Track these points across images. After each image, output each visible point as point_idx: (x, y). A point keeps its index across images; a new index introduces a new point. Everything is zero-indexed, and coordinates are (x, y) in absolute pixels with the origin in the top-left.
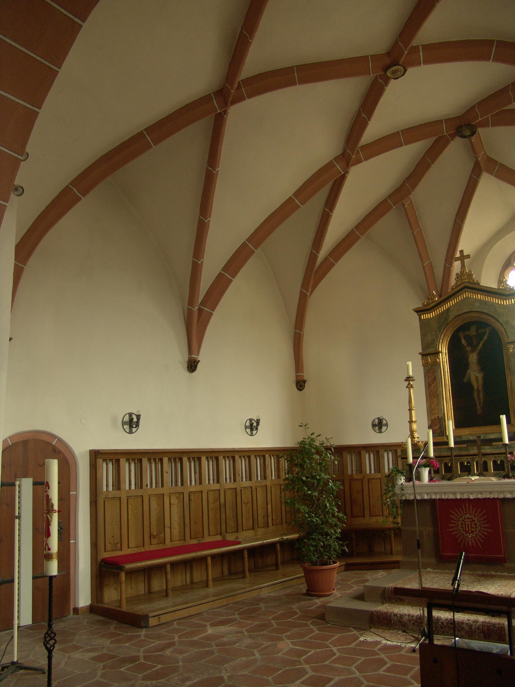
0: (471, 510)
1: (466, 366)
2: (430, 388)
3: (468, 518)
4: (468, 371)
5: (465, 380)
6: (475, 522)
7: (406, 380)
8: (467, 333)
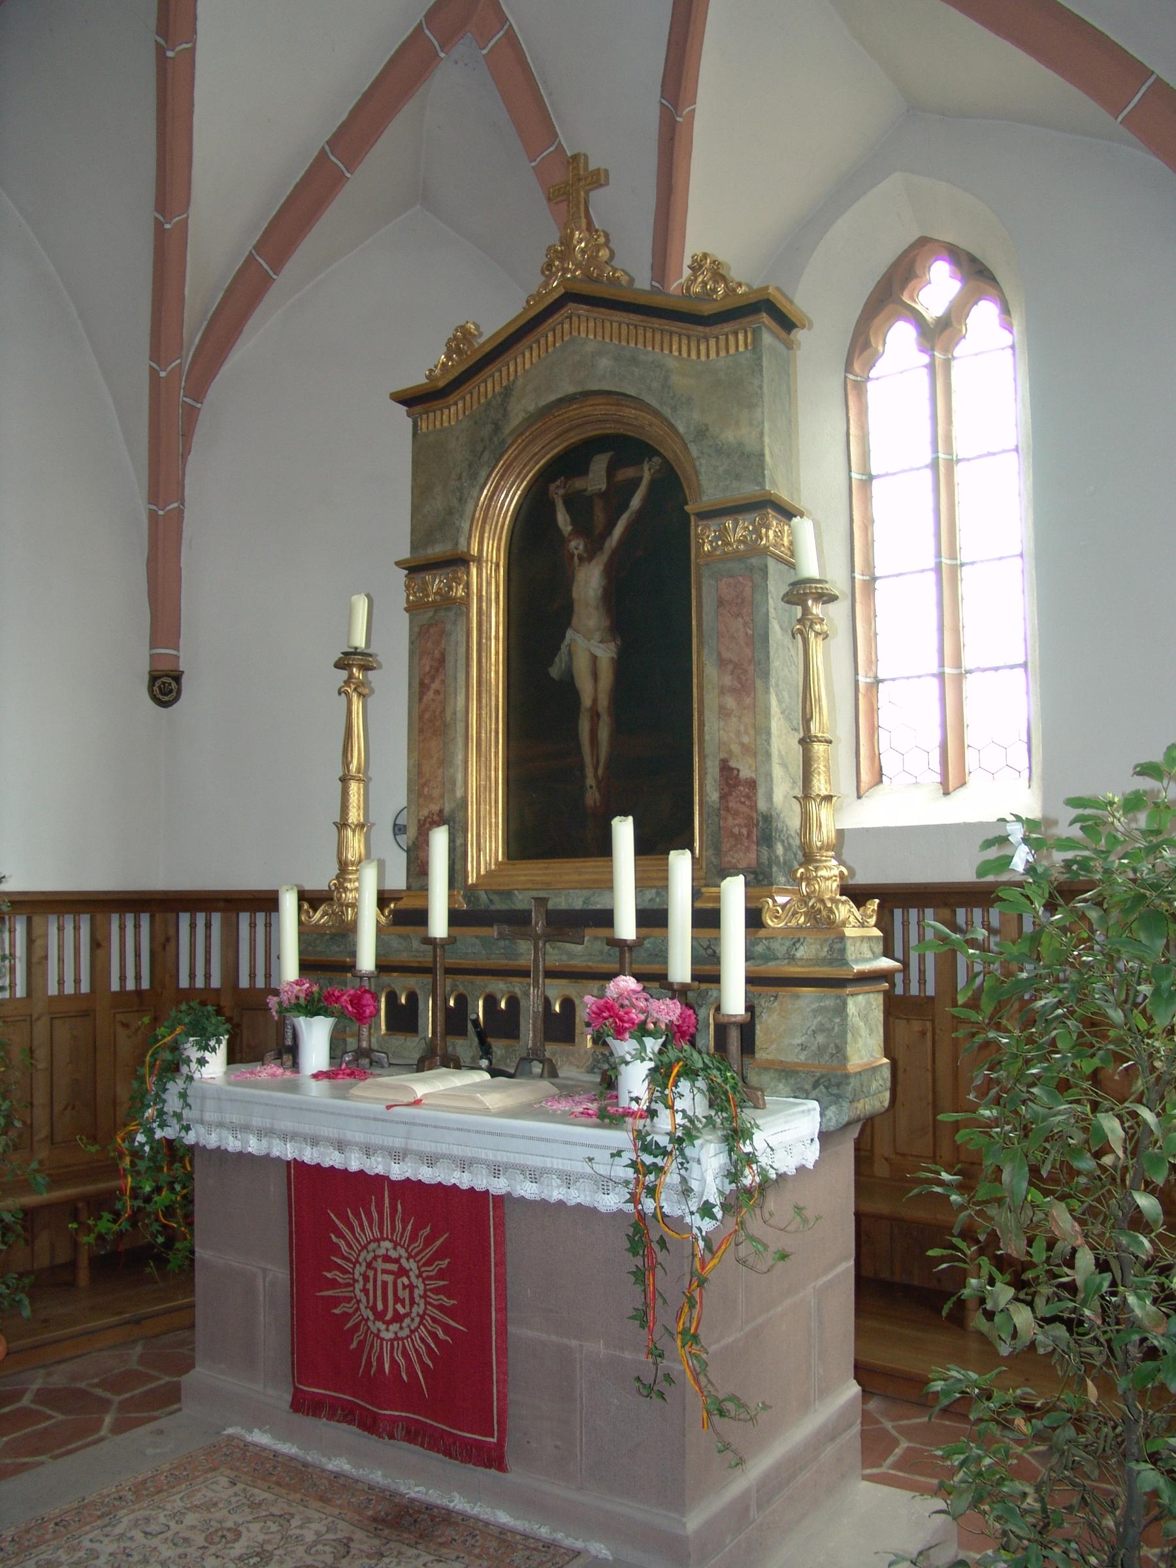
0: (399, 1225)
1: (564, 616)
2: (425, 699)
3: (387, 1259)
4: (569, 634)
5: (555, 672)
6: (408, 1277)
7: (339, 665)
8: (578, 484)
